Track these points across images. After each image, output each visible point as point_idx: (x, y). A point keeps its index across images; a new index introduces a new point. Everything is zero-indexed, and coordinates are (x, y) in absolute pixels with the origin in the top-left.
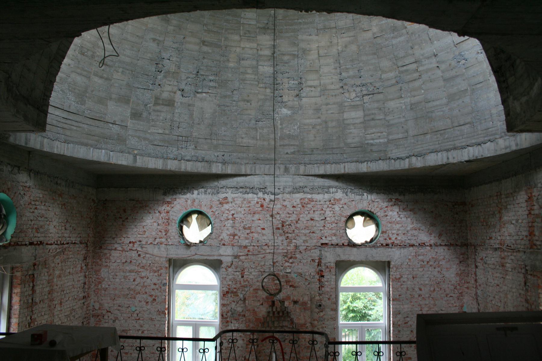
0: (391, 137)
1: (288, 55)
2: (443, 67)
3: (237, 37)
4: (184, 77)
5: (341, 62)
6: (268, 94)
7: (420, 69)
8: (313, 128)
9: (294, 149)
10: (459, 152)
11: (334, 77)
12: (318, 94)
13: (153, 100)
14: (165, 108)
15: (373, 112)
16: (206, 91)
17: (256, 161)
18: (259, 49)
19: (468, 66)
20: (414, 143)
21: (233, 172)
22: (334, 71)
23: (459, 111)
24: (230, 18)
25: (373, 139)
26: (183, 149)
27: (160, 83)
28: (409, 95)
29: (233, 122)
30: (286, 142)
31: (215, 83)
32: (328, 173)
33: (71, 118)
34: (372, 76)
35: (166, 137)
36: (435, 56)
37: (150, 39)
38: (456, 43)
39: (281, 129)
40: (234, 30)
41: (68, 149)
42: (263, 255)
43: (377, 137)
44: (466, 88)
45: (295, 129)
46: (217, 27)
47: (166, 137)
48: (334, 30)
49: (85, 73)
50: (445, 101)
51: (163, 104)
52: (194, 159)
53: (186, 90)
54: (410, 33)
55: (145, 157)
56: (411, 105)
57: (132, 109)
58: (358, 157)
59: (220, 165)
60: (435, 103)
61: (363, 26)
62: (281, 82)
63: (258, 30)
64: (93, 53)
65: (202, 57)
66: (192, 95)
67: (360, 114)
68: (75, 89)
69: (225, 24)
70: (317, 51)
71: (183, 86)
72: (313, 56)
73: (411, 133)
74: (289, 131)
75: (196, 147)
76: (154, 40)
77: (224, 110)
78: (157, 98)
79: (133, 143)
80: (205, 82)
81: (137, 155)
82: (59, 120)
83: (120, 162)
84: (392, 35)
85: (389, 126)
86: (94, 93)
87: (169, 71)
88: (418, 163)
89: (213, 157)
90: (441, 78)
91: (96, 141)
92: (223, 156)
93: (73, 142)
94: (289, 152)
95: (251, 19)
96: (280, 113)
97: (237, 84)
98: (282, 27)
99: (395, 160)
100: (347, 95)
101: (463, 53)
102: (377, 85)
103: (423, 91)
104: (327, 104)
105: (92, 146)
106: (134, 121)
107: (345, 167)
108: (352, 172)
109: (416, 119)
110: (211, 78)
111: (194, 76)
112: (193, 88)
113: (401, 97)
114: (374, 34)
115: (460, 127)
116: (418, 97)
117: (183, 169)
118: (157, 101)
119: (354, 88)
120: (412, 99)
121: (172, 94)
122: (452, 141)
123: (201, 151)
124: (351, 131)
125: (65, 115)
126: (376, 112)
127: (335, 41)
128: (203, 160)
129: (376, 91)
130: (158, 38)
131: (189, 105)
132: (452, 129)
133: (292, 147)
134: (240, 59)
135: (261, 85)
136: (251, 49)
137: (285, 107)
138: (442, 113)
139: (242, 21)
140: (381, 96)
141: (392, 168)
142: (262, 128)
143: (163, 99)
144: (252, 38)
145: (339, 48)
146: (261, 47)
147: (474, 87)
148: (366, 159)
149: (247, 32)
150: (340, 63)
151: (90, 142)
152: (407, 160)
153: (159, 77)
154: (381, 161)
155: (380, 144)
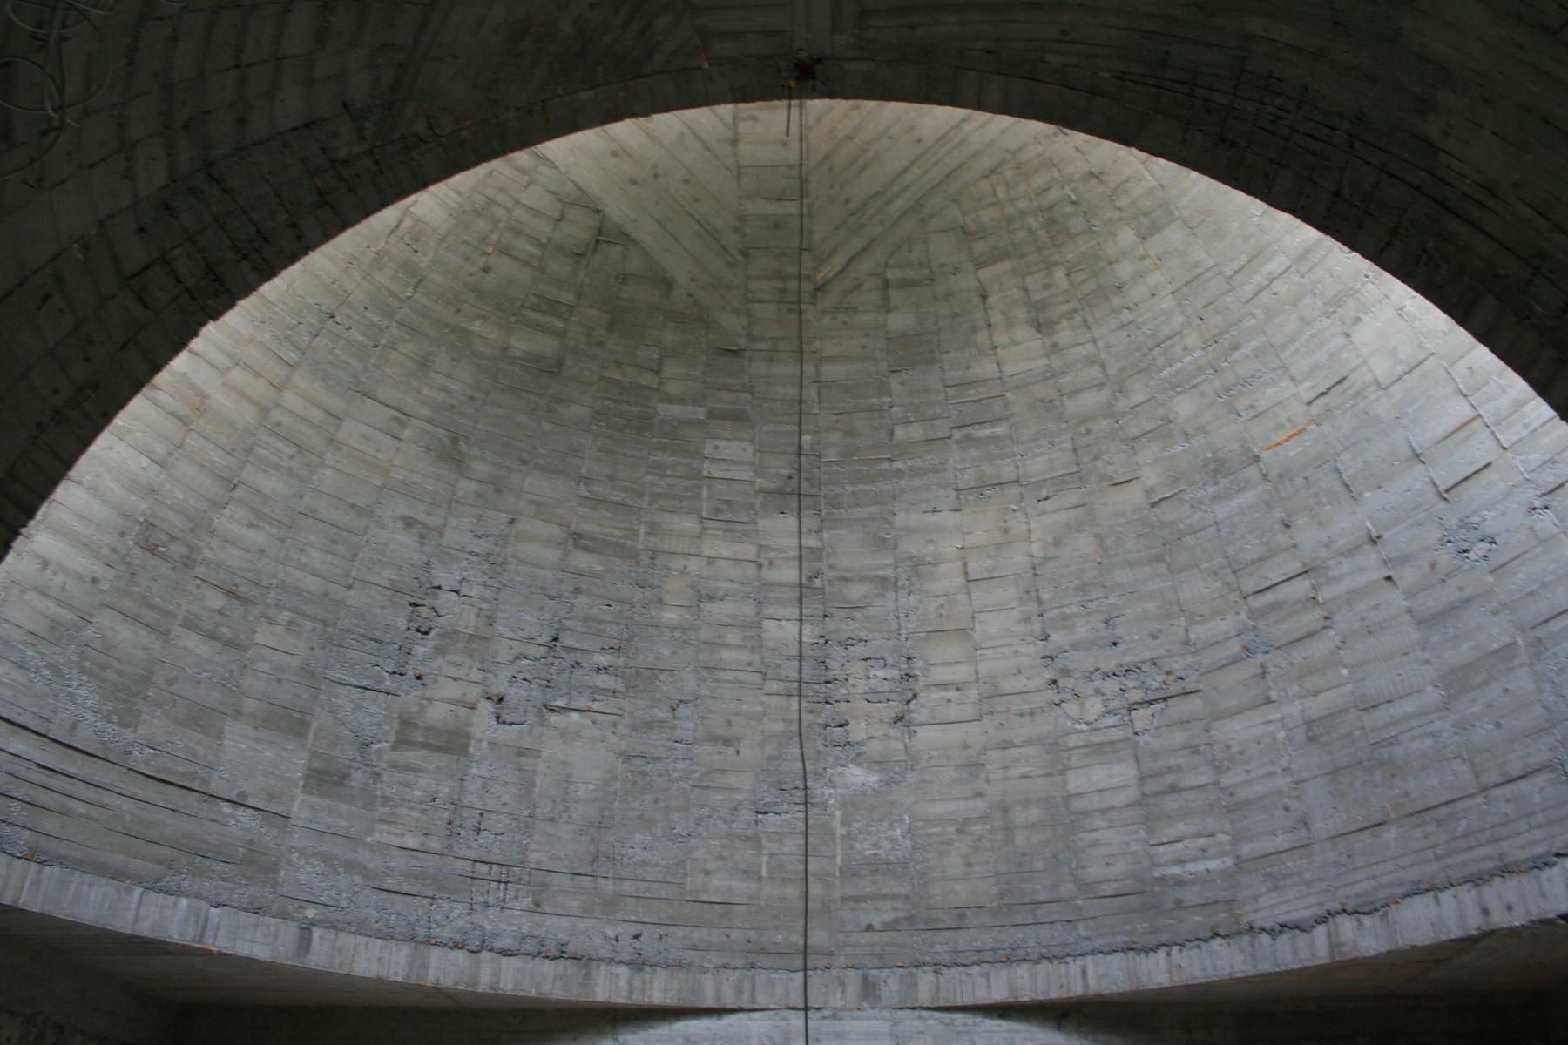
0: (1246, 849)
1: (864, 580)
2: (1407, 576)
3: (689, 524)
4: (505, 655)
5: (1046, 596)
7: (1326, 594)
8: (959, 831)
9: (895, 909)
10: (1527, 882)
11: (1023, 649)
12: (969, 711)
13: (391, 730)
14: (434, 760)
15: (1172, 762)
17: (757, 956)
18: (765, 563)
19: (1501, 561)
20: (1337, 864)
21: (671, 1000)
22: (1020, 628)
24: (665, 458)
25: (1180, 862)
26: (491, 911)
27: (422, 670)
28: (1296, 689)
29: (675, 816)
30: (865, 886)
31: (613, 678)
32: (1025, 996)
33: (73, 770)
34: (1155, 637)
35: (431, 863)
36: (1374, 541)
38: (1442, 488)
39: (848, 838)
41: (37, 883)
43: (1194, 853)
44: (1507, 640)
45: (893, 840)
46: (625, 490)
47: (431, 863)
48: (1014, 491)
49: (150, 616)
50: (1432, 696)
51: (425, 746)
52: (529, 946)
53: (511, 700)
54: (1273, 474)
55: (342, 935)
56: (1309, 723)
57: (314, 755)
58: (1132, 932)
59: (623, 971)
60: (1398, 709)
61: (1109, 470)
62: (840, 674)
63: (759, 500)
64: (191, 549)
65: (571, 588)
66: (531, 718)
68: (103, 667)
69: (650, 478)
70: (960, 564)
71: (500, 686)
72: (948, 580)
73: (1321, 827)
74: (876, 846)
75: (537, 904)
76: (409, 523)
77: (644, 774)
78: (407, 723)
79: (303, 877)
80: (578, 672)
82: (23, 773)
83: (243, 950)
84: (1211, 490)
85: (1236, 808)
86: (174, 689)
87: (455, 632)
88: (1365, 939)
89: (598, 941)
90: (1407, 618)
91: (161, 863)
92: (637, 937)
93: (62, 861)
94: (876, 921)
95: (734, 462)
96: (837, 780)
97: (689, 683)
98: (838, 489)
99: (1271, 932)
100: (1071, 708)
101: (1474, 519)
102: (1175, 666)
103: (1345, 672)
104: (1005, 746)
105: (139, 880)
106: (315, 800)
107: (1084, 972)
108: (1115, 989)
109: (1333, 773)
110: (602, 659)
112: (536, 693)
113: (1269, 701)
114: (1149, 492)
115: (1513, 787)
116: (1329, 695)
117: (484, 984)
118: (407, 732)
119: (1097, 683)
120: (1310, 702)
121: (463, 712)
123: (554, 919)
124: (1097, 835)
125: (51, 756)
126: (1181, 760)
127: (1019, 526)
128: (561, 954)
129: (1175, 688)
130: (422, 517)
131: (521, 752)
132: (1480, 799)
133: (888, 904)
134: (702, 597)
135: (773, 686)
136: (739, 561)
137: (858, 759)
138: (1429, 742)
139: (708, 469)
140: (1193, 705)
141: (1264, 967)
142: (778, 837)
143: (428, 729)
144: (740, 527)
145: (1035, 549)
146: (772, 555)
147: (1539, 633)
148: (1165, 937)
149: (724, 507)
150: (1039, 601)
151: (136, 864)
152: (1321, 930)
153: (419, 650)
154: (1218, 941)
155: (1209, 878)
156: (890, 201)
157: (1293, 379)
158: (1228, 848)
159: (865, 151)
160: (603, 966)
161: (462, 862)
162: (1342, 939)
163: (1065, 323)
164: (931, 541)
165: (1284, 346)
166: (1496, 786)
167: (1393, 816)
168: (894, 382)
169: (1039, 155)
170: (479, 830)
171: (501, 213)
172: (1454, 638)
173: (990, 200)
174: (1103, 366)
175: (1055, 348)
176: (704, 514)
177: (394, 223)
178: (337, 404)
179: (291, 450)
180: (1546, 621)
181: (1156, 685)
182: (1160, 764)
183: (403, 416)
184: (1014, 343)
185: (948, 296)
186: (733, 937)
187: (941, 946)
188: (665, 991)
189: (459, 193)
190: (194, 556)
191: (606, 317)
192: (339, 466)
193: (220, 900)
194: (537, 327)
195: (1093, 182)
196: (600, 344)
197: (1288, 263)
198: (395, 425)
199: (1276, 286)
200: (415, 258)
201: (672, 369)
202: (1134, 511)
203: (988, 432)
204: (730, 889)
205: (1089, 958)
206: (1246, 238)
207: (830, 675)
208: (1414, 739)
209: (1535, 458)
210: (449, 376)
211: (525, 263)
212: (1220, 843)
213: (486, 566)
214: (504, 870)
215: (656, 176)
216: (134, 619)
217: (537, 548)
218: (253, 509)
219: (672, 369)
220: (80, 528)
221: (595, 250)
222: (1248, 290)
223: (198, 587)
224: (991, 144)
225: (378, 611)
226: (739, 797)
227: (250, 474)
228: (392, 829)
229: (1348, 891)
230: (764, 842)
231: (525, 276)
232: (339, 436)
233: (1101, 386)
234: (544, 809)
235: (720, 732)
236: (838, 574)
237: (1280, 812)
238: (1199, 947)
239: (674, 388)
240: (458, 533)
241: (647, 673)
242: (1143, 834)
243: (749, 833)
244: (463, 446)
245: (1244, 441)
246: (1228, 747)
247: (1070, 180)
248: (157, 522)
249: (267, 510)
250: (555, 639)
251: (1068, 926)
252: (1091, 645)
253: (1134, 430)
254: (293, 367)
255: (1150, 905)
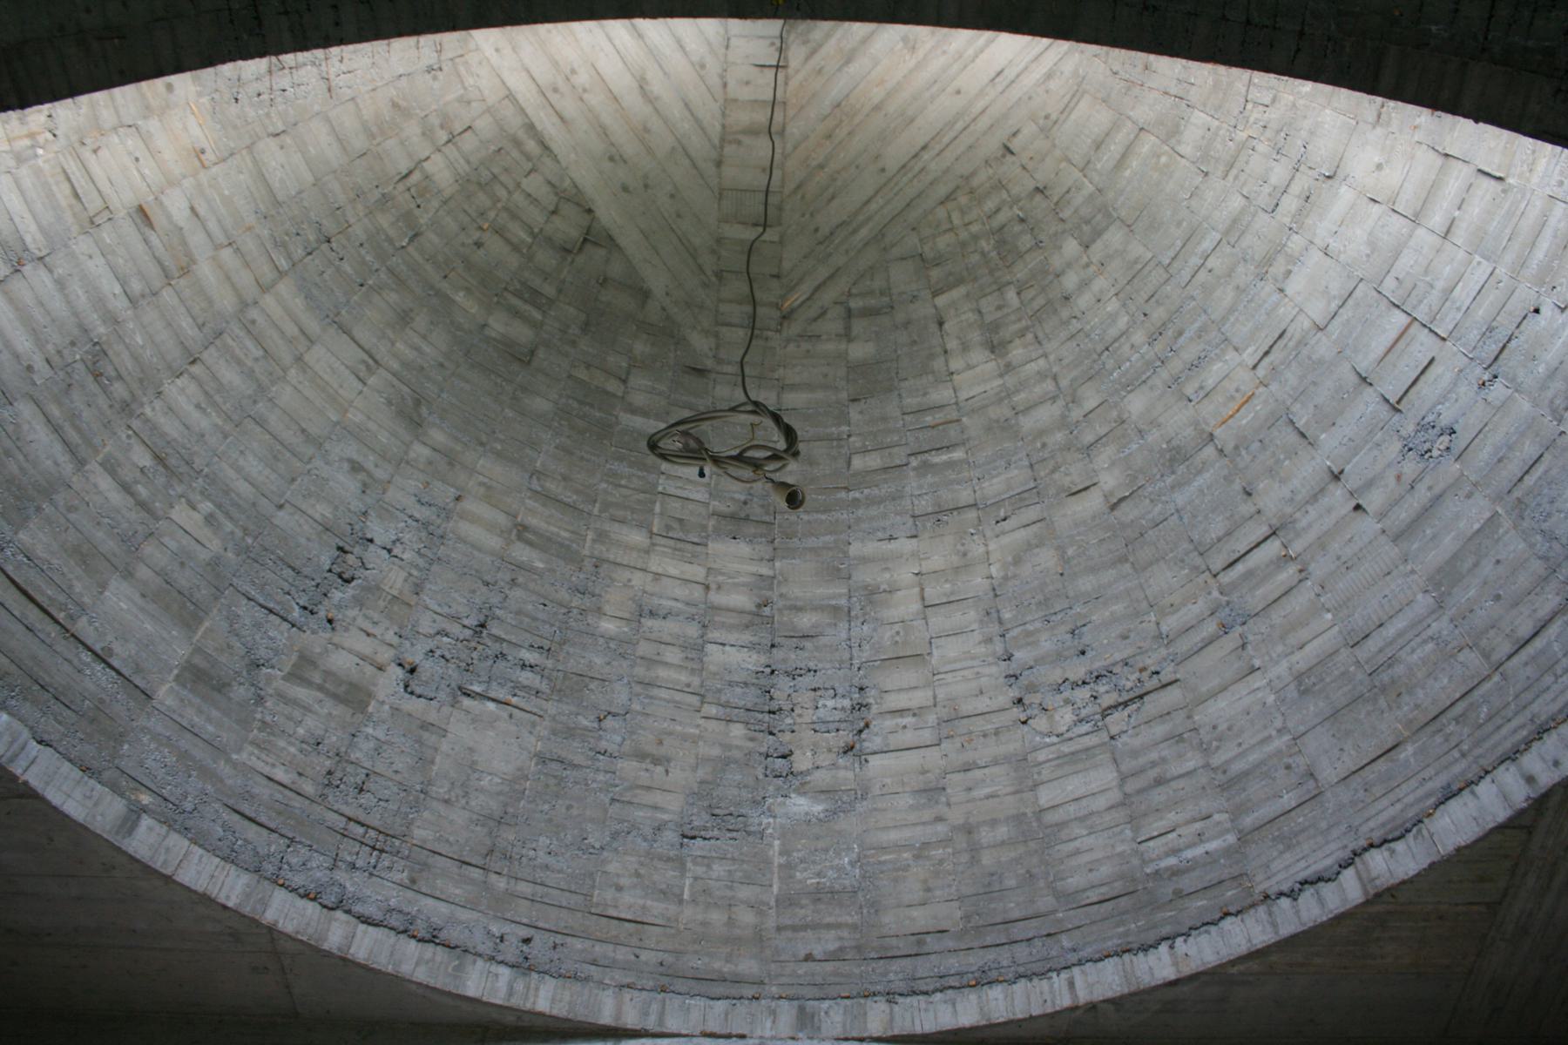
0: (1248, 821)
1: (815, 609)
3: (638, 538)
4: (426, 626)
5: (1007, 615)
6: (736, 742)
8: (917, 857)
11: (987, 670)
15: (1154, 756)
16: (501, 694)
22: (982, 649)
23: (1497, 598)
29: (589, 827)
30: (806, 913)
34: (1126, 638)
36: (1336, 477)
37: (341, 459)
39: (788, 867)
40: (633, 511)
42: (975, 794)
43: (1189, 835)
44: (1488, 515)
45: (840, 869)
46: (577, 492)
48: (972, 515)
50: (1424, 602)
51: (320, 688)
54: (1229, 448)
57: (198, 650)
58: (1126, 934)
59: (505, 972)
60: (1390, 631)
61: (1067, 481)
63: (712, 523)
65: (508, 577)
66: (442, 696)
67: (1103, 777)
69: (604, 485)
70: (917, 590)
71: (415, 655)
72: (905, 606)
74: (819, 875)
75: (413, 881)
76: (356, 467)
79: (149, 763)
80: (501, 664)
81: (144, 810)
85: (1230, 784)
86: (72, 516)
87: (378, 588)
88: (1399, 863)
89: (479, 935)
90: (1383, 539)
92: (527, 941)
94: (818, 951)
96: (778, 810)
99: (1292, 894)
100: (1040, 723)
101: (1430, 418)
102: (1149, 662)
103: (1329, 616)
107: (1071, 984)
110: (530, 657)
111: (468, 633)
112: (452, 670)
115: (1530, 650)
116: (1315, 642)
122: (1516, 714)
123: (430, 901)
124: (1077, 844)
126: (1166, 751)
127: (977, 549)
128: (432, 938)
130: (369, 465)
131: (426, 726)
132: (1496, 678)
137: (801, 791)
138: (1430, 646)
140: (1173, 696)
144: (689, 547)
146: (720, 578)
148: (1166, 930)
149: (676, 525)
150: (1000, 622)
152: (1349, 874)
153: (337, 595)
154: (1229, 919)
156: (855, 231)
157: (1236, 349)
158: (1229, 825)
159: (834, 180)
160: (480, 963)
161: (336, 816)
162: (1374, 874)
163: (1017, 342)
164: (887, 569)
165: (1225, 319)
166: (1510, 657)
167: (1406, 734)
168: (854, 413)
169: (990, 178)
170: (361, 790)
171: (502, 193)
172: (1434, 537)
173: (945, 226)
174: (1055, 378)
175: (1009, 368)
176: (655, 530)
177: (405, 172)
178: (313, 326)
179: (260, 353)
180: (1521, 479)
181: (1129, 685)
182: (1142, 761)
183: (373, 362)
184: (969, 367)
185: (907, 324)
186: (643, 958)
187: (896, 973)
188: (553, 1001)
189: (468, 162)
190: (133, 406)
191: (583, 317)
192: (300, 387)
193: (46, 737)
194: (516, 313)
195: (1038, 197)
196: (573, 343)
197: (1218, 237)
198: (362, 367)
199: (1210, 263)
200: (417, 212)
201: (639, 381)
202: (1094, 518)
203: (944, 457)
204: (644, 907)
205: (1076, 971)
206: (1179, 224)
207: (774, 706)
208: (1413, 651)
209: (1474, 335)
210: (424, 337)
211: (516, 248)
212: (1219, 823)
213: (424, 534)
214: (381, 837)
215: (646, 186)
216: (56, 429)
217: (479, 528)
218: (206, 393)
219: (639, 381)
220: (37, 314)
221: (581, 249)
222: (1186, 275)
223: (129, 437)
224: (947, 170)
225: (303, 541)
226: (666, 817)
227: (210, 356)
228: (263, 756)
229: (1372, 824)
230: (689, 865)
231: (514, 261)
232: (307, 358)
233: (1054, 399)
234: (440, 790)
235: (651, 749)
236: (789, 603)
237: (1282, 772)
238: (1208, 932)
239: (639, 399)
240: (402, 493)
241: (576, 678)
242: (1128, 832)
243: (672, 854)
244: (424, 410)
245: (1196, 424)
246: (1215, 727)
247: (1016, 200)
248: (110, 353)
249: (217, 398)
250: (483, 626)
251: (1049, 941)
252: (1059, 657)
253: (1089, 438)
254: (282, 274)
255: (1146, 905)
